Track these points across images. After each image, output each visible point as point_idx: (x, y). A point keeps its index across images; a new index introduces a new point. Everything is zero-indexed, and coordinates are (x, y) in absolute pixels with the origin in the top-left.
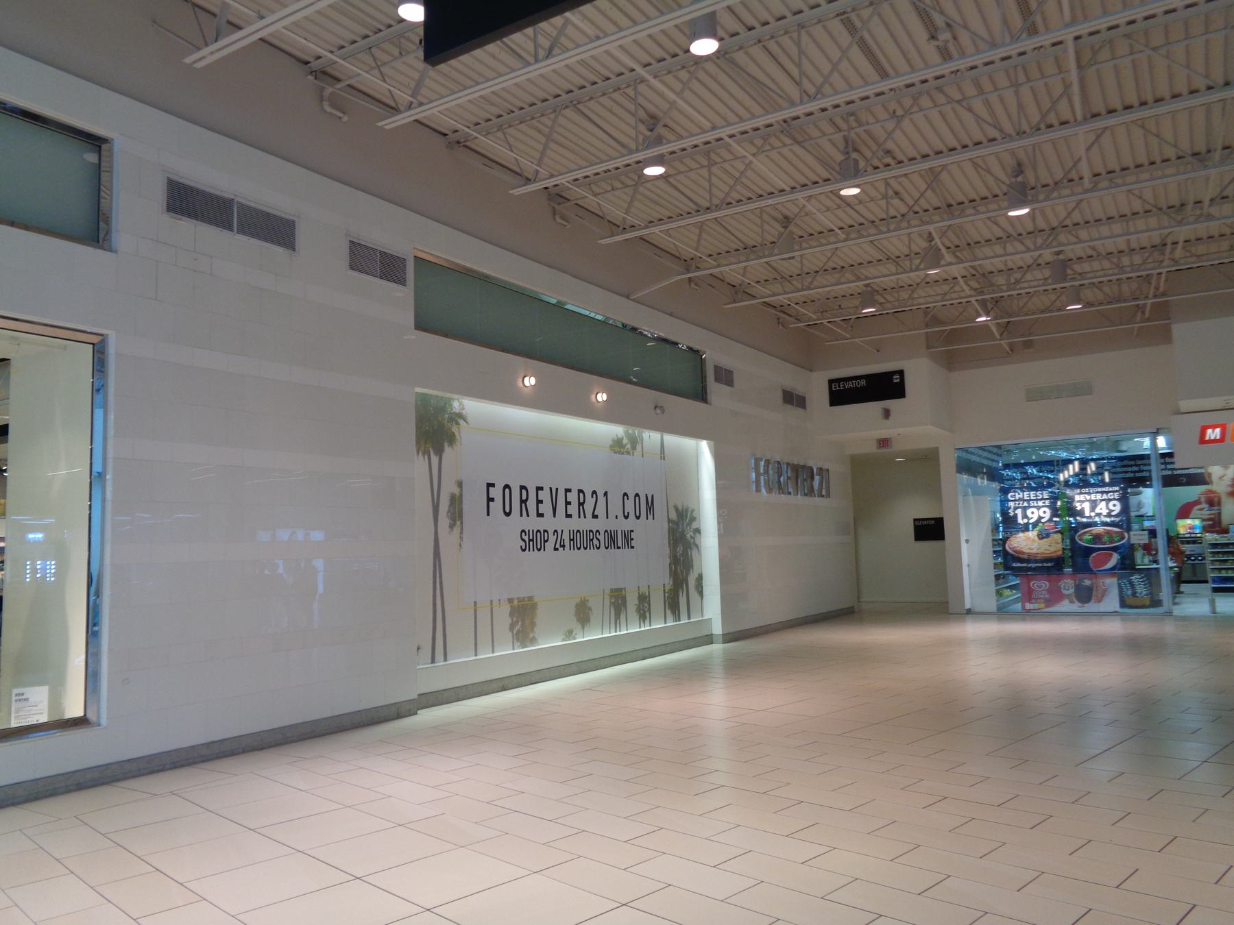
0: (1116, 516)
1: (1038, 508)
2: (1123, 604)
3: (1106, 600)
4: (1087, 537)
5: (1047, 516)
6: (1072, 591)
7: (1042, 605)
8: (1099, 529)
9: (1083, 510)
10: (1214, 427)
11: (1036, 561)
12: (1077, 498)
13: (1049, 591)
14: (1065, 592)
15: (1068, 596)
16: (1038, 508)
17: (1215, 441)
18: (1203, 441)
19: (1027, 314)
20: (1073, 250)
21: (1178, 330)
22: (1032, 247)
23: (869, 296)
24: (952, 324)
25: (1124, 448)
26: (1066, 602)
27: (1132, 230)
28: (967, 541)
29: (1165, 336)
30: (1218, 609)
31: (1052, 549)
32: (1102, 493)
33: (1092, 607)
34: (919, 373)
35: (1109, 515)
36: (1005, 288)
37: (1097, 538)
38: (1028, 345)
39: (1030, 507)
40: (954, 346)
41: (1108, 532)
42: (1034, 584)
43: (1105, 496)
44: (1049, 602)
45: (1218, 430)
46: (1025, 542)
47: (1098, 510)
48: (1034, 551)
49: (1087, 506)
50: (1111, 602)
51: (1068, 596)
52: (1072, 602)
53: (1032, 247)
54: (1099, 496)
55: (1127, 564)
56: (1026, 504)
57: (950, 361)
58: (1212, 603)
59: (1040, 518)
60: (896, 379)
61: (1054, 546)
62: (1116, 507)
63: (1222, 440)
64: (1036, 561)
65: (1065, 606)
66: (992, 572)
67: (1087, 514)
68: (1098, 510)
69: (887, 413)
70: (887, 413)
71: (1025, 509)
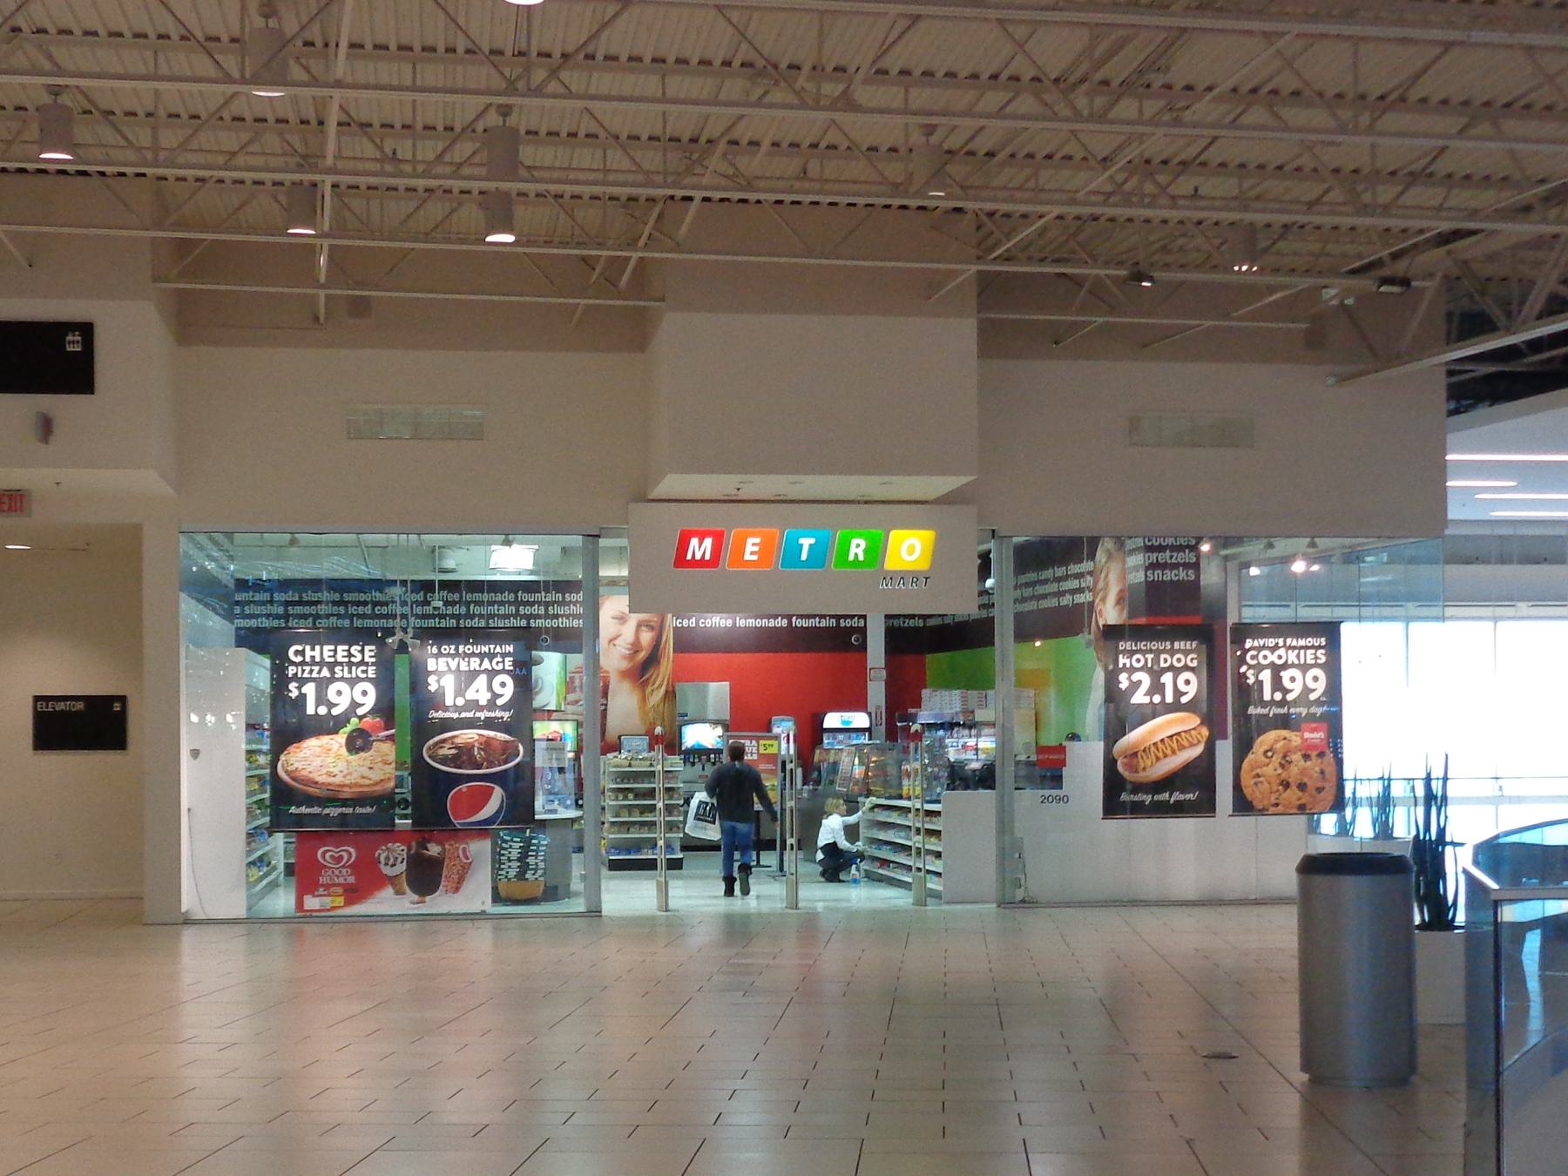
0: (504, 708)
1: (352, 682)
2: (497, 898)
3: (468, 887)
4: (446, 751)
5: (369, 701)
6: (401, 868)
7: (340, 901)
8: (468, 736)
9: (441, 693)
10: (702, 536)
11: (344, 803)
12: (431, 664)
13: (355, 867)
14: (387, 871)
15: (392, 880)
16: (352, 682)
17: (702, 563)
18: (681, 560)
19: (448, 241)
20: (530, 112)
21: (678, 330)
22: (236, 74)
23: (56, 127)
24: (216, 229)
25: (450, 563)
26: (389, 891)
27: (164, 70)
28: (195, 753)
29: (634, 333)
30: (672, 904)
31: (376, 776)
32: (482, 656)
33: (440, 902)
34: (130, 336)
35: (491, 705)
36: (659, 179)
37: (463, 755)
38: (359, 307)
39: (332, 679)
40: (214, 285)
41: (487, 744)
42: (325, 854)
43: (486, 664)
44: (353, 894)
45: (708, 542)
46: (321, 760)
47: (471, 694)
48: (338, 780)
49: (449, 683)
50: (476, 895)
51: (392, 880)
52: (399, 892)
53: (236, 74)
54: (475, 663)
55: (519, 812)
56: (325, 673)
57: (190, 321)
58: (664, 891)
59: (355, 705)
60: (73, 344)
61: (377, 768)
62: (506, 689)
63: (715, 561)
64: (344, 803)
65: (385, 902)
66: (241, 826)
67: (449, 702)
68: (471, 694)
69: (46, 427)
70: (46, 427)
71: (322, 685)
